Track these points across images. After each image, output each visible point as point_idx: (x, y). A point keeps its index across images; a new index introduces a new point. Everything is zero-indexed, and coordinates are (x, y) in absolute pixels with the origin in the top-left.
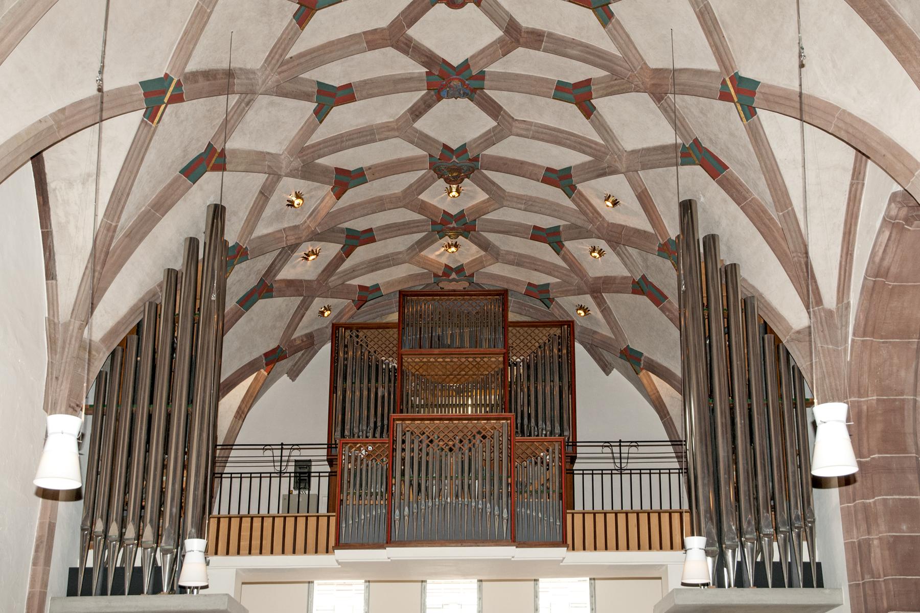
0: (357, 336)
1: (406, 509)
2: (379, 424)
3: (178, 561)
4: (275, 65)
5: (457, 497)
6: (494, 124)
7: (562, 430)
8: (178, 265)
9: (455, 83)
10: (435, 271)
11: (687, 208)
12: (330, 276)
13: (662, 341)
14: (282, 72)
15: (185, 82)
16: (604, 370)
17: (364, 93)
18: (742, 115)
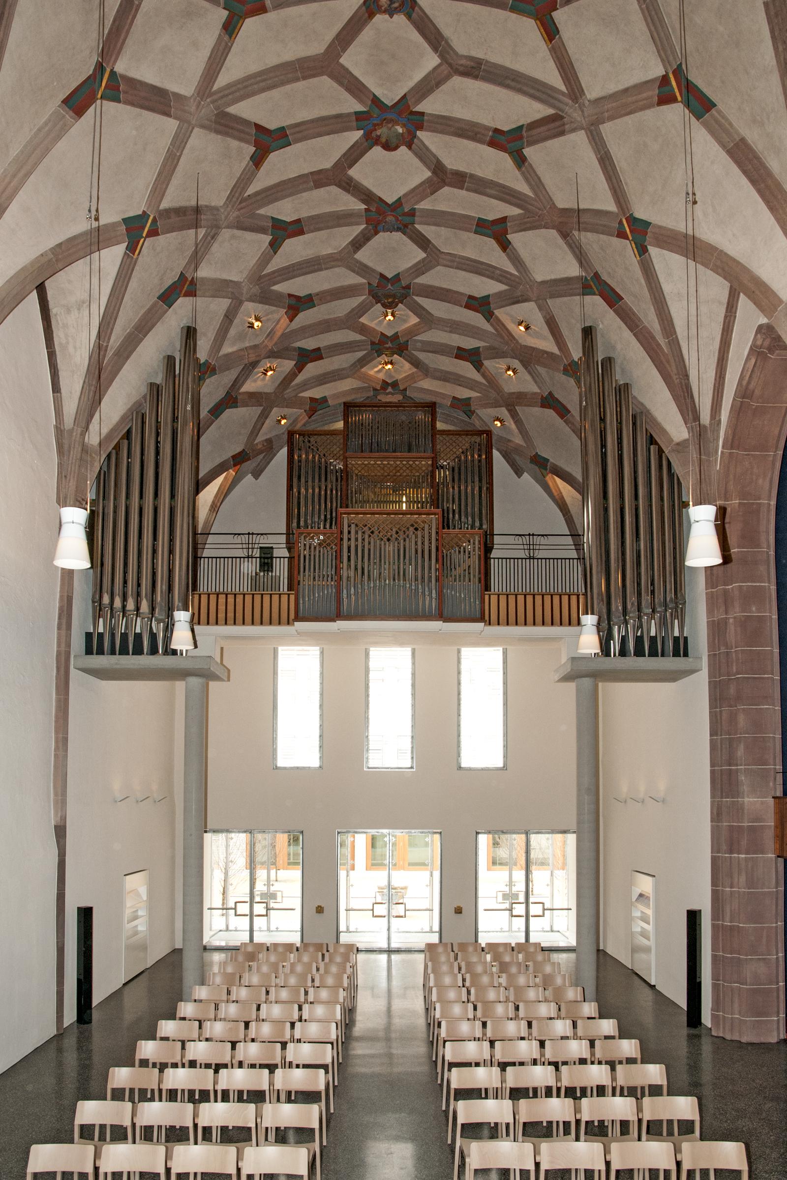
0: (309, 442)
1: (352, 589)
2: (329, 516)
3: (169, 628)
4: (235, 202)
5: (394, 580)
6: (424, 255)
7: (481, 525)
8: (159, 380)
9: (390, 219)
10: (374, 385)
11: (588, 333)
12: (285, 389)
13: (566, 450)
14: (242, 208)
15: (160, 218)
16: (517, 474)
17: (312, 228)
18: (636, 252)
